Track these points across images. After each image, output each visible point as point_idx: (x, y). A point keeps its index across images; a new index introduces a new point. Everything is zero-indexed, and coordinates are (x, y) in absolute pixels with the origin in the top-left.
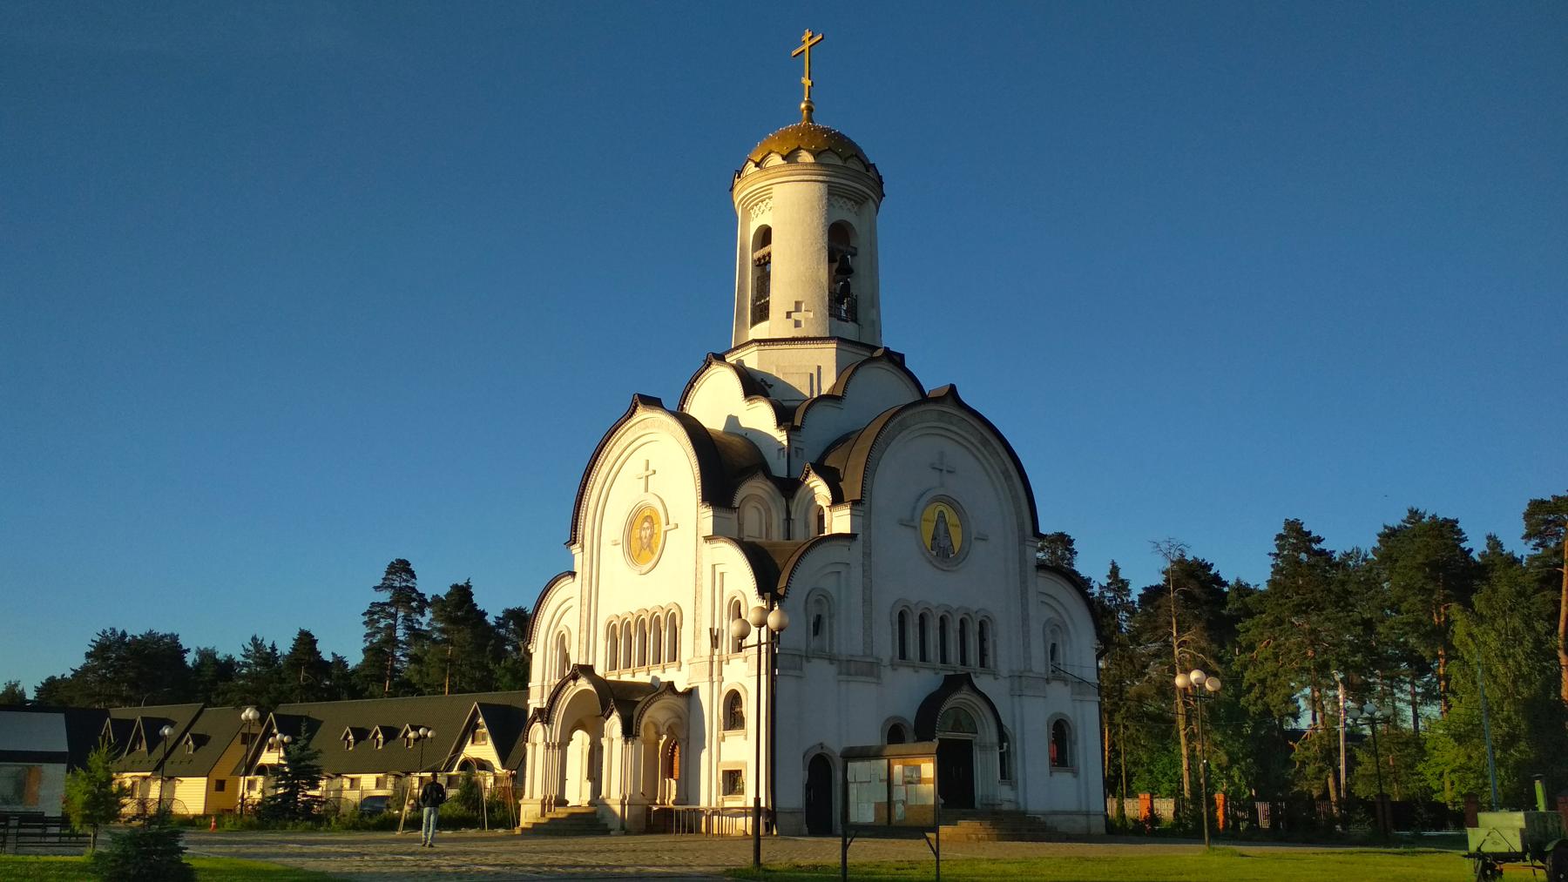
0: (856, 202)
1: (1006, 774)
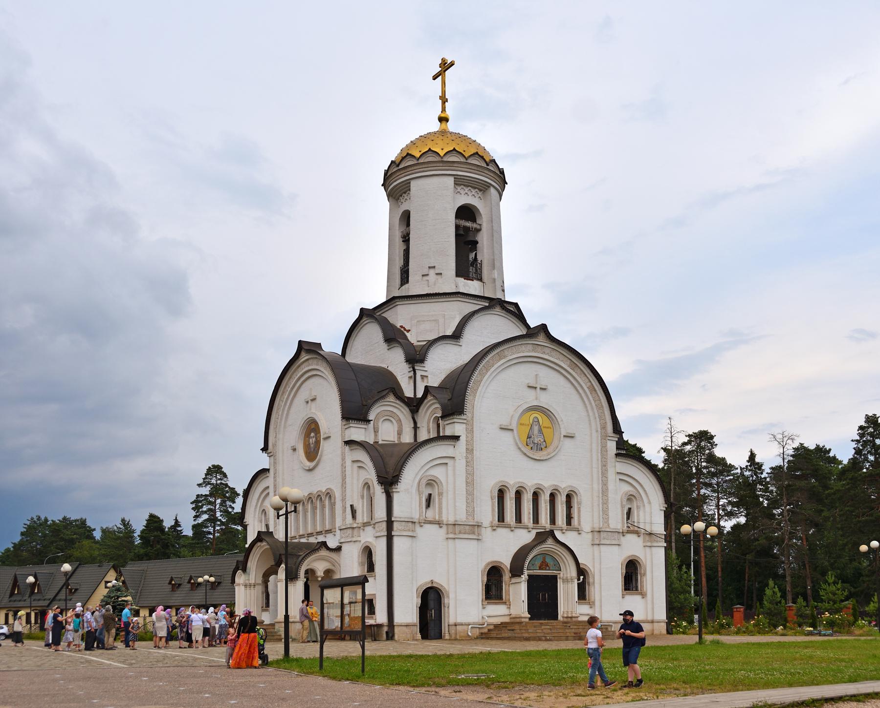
0: (481, 190)
1: (582, 594)
